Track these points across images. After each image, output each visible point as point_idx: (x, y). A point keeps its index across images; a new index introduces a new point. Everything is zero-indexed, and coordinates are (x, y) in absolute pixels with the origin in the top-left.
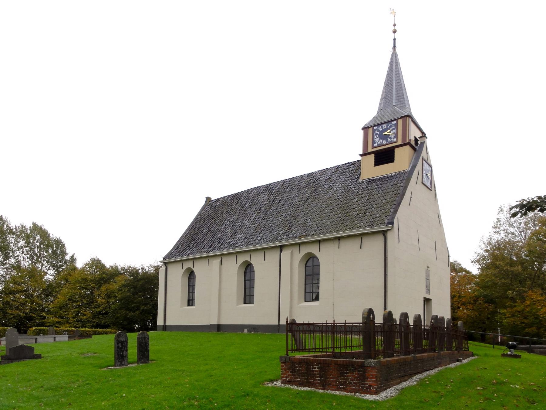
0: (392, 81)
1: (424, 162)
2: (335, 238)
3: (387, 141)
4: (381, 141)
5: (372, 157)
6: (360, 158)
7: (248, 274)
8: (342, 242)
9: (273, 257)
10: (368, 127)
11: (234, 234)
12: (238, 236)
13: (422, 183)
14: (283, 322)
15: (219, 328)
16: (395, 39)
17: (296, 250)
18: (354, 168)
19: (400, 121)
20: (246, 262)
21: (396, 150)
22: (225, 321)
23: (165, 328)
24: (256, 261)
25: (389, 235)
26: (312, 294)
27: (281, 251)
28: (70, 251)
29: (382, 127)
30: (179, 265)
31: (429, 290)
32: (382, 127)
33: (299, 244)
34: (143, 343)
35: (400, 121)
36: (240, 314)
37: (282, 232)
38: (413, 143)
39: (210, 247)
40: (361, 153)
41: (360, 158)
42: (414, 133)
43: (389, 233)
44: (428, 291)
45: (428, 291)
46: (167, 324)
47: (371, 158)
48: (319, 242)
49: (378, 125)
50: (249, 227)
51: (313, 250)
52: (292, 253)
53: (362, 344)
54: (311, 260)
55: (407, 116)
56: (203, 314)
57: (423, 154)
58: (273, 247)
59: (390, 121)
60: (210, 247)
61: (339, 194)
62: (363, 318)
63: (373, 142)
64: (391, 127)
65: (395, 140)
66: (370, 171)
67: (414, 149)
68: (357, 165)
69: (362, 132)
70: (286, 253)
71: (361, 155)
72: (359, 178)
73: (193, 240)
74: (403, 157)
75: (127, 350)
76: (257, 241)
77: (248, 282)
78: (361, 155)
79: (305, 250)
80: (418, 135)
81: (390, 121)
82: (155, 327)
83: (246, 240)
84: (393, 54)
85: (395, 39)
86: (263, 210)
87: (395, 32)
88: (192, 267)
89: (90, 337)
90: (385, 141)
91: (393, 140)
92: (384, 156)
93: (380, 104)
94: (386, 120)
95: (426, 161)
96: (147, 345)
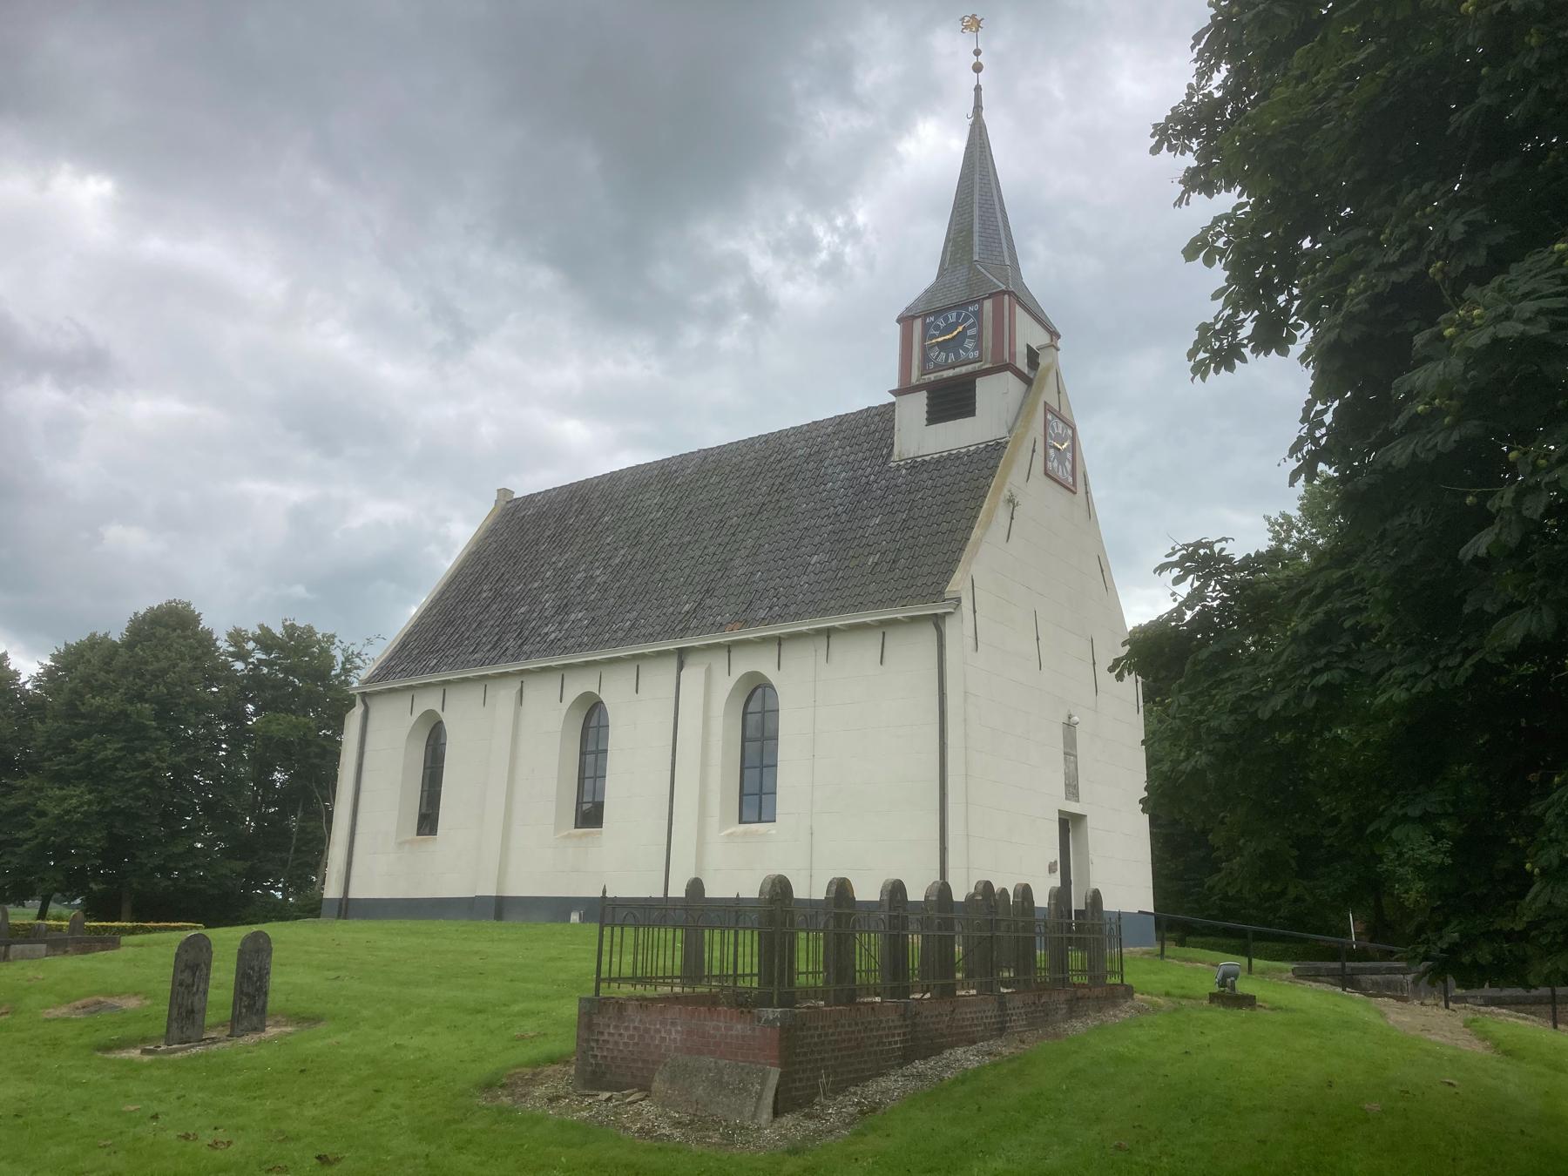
0: (971, 194)
1: (1049, 417)
2: (818, 632)
3: (957, 355)
4: (943, 355)
5: (921, 398)
6: (892, 399)
7: (592, 733)
8: (835, 641)
9: (659, 678)
10: (914, 317)
11: (564, 608)
12: (573, 617)
13: (1046, 474)
14: (678, 890)
15: (500, 908)
16: (978, 89)
17: (719, 662)
18: (874, 427)
19: (988, 304)
20: (587, 696)
21: (979, 382)
22: (521, 886)
23: (347, 908)
24: (615, 692)
25: (950, 628)
26: (756, 795)
27: (681, 667)
28: (205, 623)
29: (946, 319)
30: (402, 703)
31: (1076, 787)
32: (946, 319)
33: (729, 647)
34: (252, 968)
35: (988, 304)
36: (548, 863)
37: (687, 607)
38: (1022, 363)
39: (494, 648)
40: (896, 386)
41: (892, 399)
42: (1027, 334)
43: (949, 622)
44: (1072, 790)
45: (1072, 790)
46: (351, 896)
47: (920, 401)
48: (779, 640)
49: (938, 313)
50: (604, 589)
51: (763, 664)
52: (709, 671)
53: (756, 971)
54: (759, 691)
55: (1004, 292)
56: (454, 867)
57: (1049, 395)
58: (660, 654)
59: (964, 305)
60: (494, 648)
61: (837, 501)
62: (761, 893)
63: (925, 359)
64: (967, 318)
65: (977, 353)
66: (919, 437)
67: (1028, 381)
68: (884, 415)
69: (898, 327)
70: (693, 675)
71: (893, 392)
72: (890, 454)
73: (450, 623)
74: (996, 397)
75: (205, 993)
76: (620, 634)
77: (590, 758)
78: (893, 392)
79: (744, 664)
80: (1038, 338)
81: (964, 305)
82: (313, 908)
83: (593, 630)
84: (973, 126)
85: (978, 89)
86: (646, 539)
87: (978, 68)
88: (439, 711)
89: (115, 944)
90: (952, 356)
91: (972, 355)
92: (951, 400)
93: (944, 252)
94: (955, 300)
95: (1059, 416)
96: (263, 974)
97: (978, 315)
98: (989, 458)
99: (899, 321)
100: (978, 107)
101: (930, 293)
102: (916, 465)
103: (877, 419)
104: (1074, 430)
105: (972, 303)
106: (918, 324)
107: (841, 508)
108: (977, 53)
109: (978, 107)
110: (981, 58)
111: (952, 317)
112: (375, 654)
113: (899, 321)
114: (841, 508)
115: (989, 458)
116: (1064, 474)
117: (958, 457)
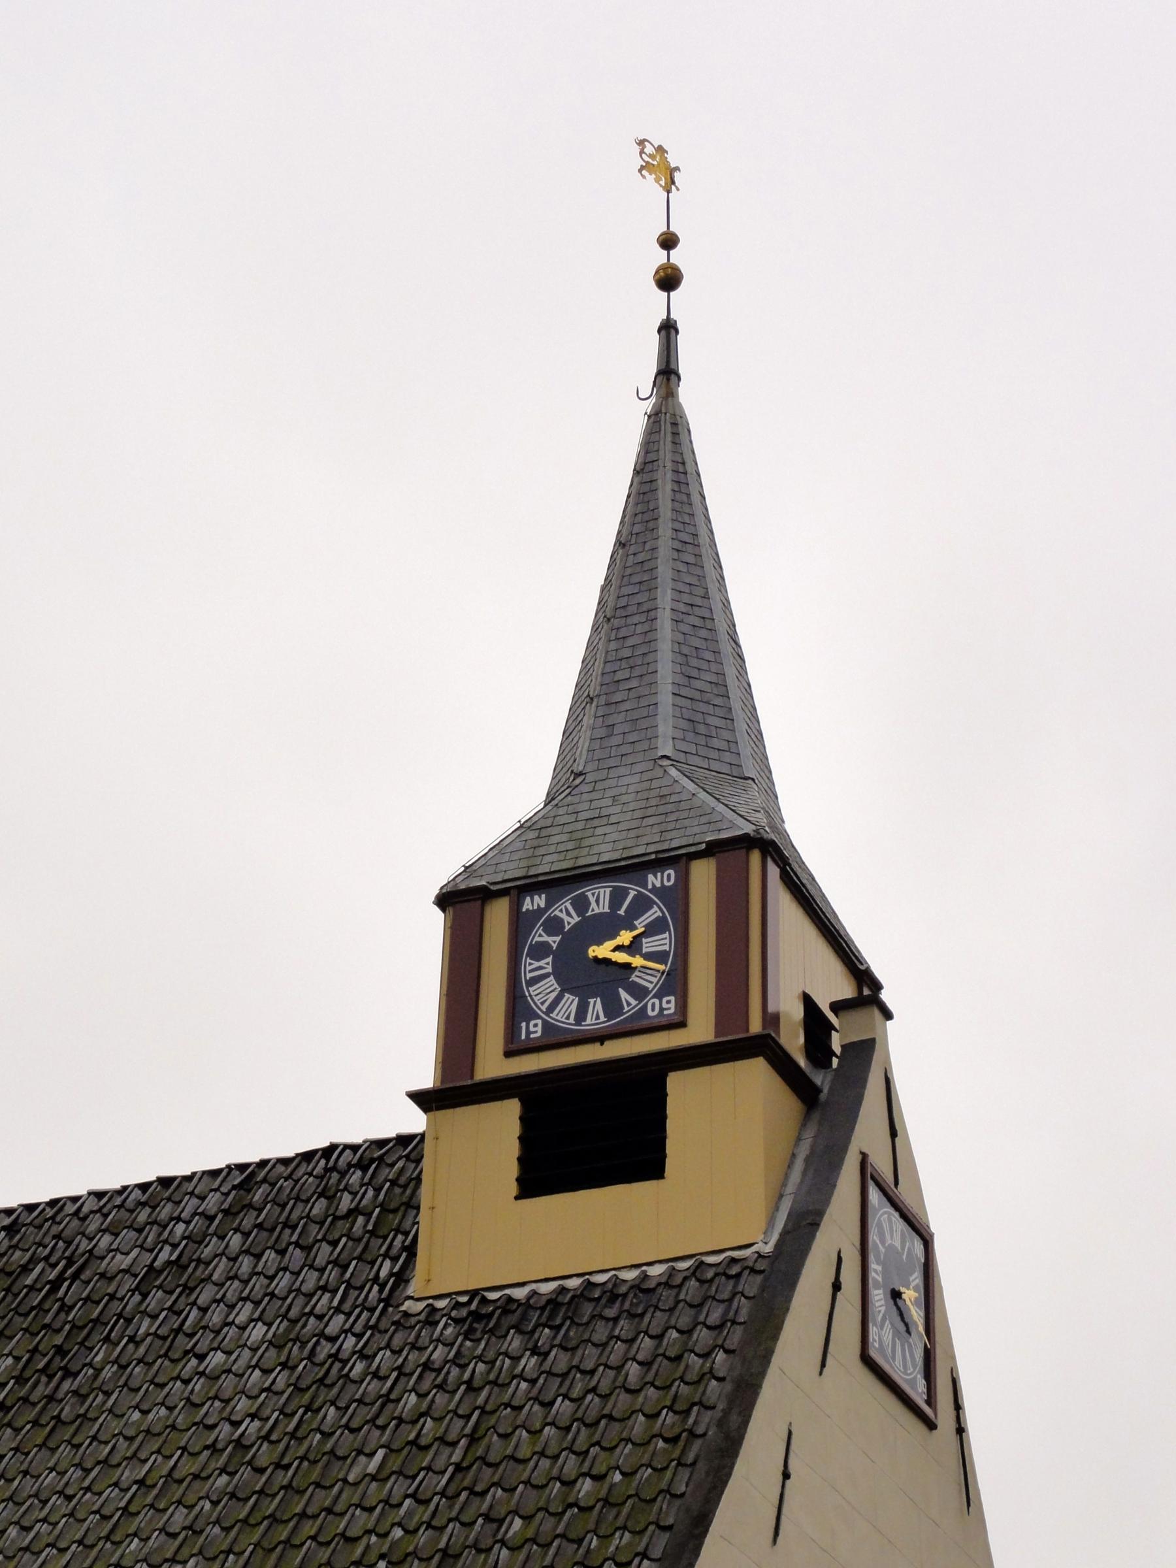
0: (649, 586)
4: (571, 1003)
5: (506, 1116)
6: (415, 1121)
10: (485, 895)
16: (668, 328)
18: (351, 1198)
21: (678, 1084)
29: (581, 905)
32: (581, 905)
35: (703, 875)
38: (794, 1041)
40: (426, 1080)
41: (415, 1121)
42: (798, 973)
57: (867, 1134)
65: (670, 1005)
66: (490, 1231)
69: (437, 919)
71: (422, 1099)
72: (402, 1278)
78: (422, 1099)
81: (636, 868)
85: (668, 328)
87: (668, 280)
90: (596, 1006)
92: (593, 1128)
97: (678, 901)
98: (740, 1301)
99: (445, 900)
100: (667, 374)
101: (532, 831)
102: (483, 1314)
103: (356, 1177)
104: (927, 1242)
105: (659, 863)
106: (498, 915)
107: (252, 1428)
108: (668, 242)
109: (667, 374)
110: (677, 256)
111: (599, 898)
112: (644, 950)
113: (445, 900)
114: (252, 1428)
115: (740, 1301)
116: (906, 1369)
117: (613, 1293)
